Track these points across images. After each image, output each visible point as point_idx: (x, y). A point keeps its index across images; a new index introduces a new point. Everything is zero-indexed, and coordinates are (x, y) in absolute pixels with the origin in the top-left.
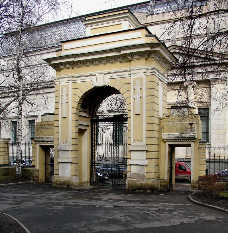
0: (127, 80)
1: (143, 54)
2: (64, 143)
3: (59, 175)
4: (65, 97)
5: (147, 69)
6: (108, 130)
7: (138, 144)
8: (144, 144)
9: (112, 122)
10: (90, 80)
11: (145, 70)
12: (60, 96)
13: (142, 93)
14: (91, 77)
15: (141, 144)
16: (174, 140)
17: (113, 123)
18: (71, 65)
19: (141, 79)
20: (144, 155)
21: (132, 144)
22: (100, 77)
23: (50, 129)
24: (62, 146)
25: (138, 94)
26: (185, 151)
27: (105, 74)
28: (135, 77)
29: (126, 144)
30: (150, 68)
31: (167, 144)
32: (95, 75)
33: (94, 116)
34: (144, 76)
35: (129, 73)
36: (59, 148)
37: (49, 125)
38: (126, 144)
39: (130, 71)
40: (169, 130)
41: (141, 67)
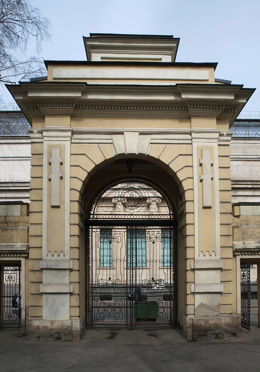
0: (185, 149)
1: (217, 108)
2: (56, 257)
3: (44, 318)
4: (56, 166)
5: (221, 135)
6: (117, 239)
7: (208, 257)
8: (218, 257)
9: (124, 226)
10: (110, 141)
11: (217, 135)
12: (45, 163)
13: (213, 173)
14: (112, 136)
15: (213, 257)
16: (254, 252)
17: (125, 227)
18: (70, 109)
19: (211, 149)
20: (216, 276)
21: (197, 258)
22: (132, 138)
23: (12, 230)
24: (49, 259)
25: (207, 173)
26: (252, 269)
27: (141, 134)
28: (201, 144)
29: (115, 261)
30: (225, 134)
31: (238, 258)
32: (122, 133)
33: (92, 214)
34: (215, 145)
35: (188, 137)
36: (43, 264)
37: (9, 224)
38: (115, 261)
39: (190, 134)
40: (243, 237)
41: (210, 129)
